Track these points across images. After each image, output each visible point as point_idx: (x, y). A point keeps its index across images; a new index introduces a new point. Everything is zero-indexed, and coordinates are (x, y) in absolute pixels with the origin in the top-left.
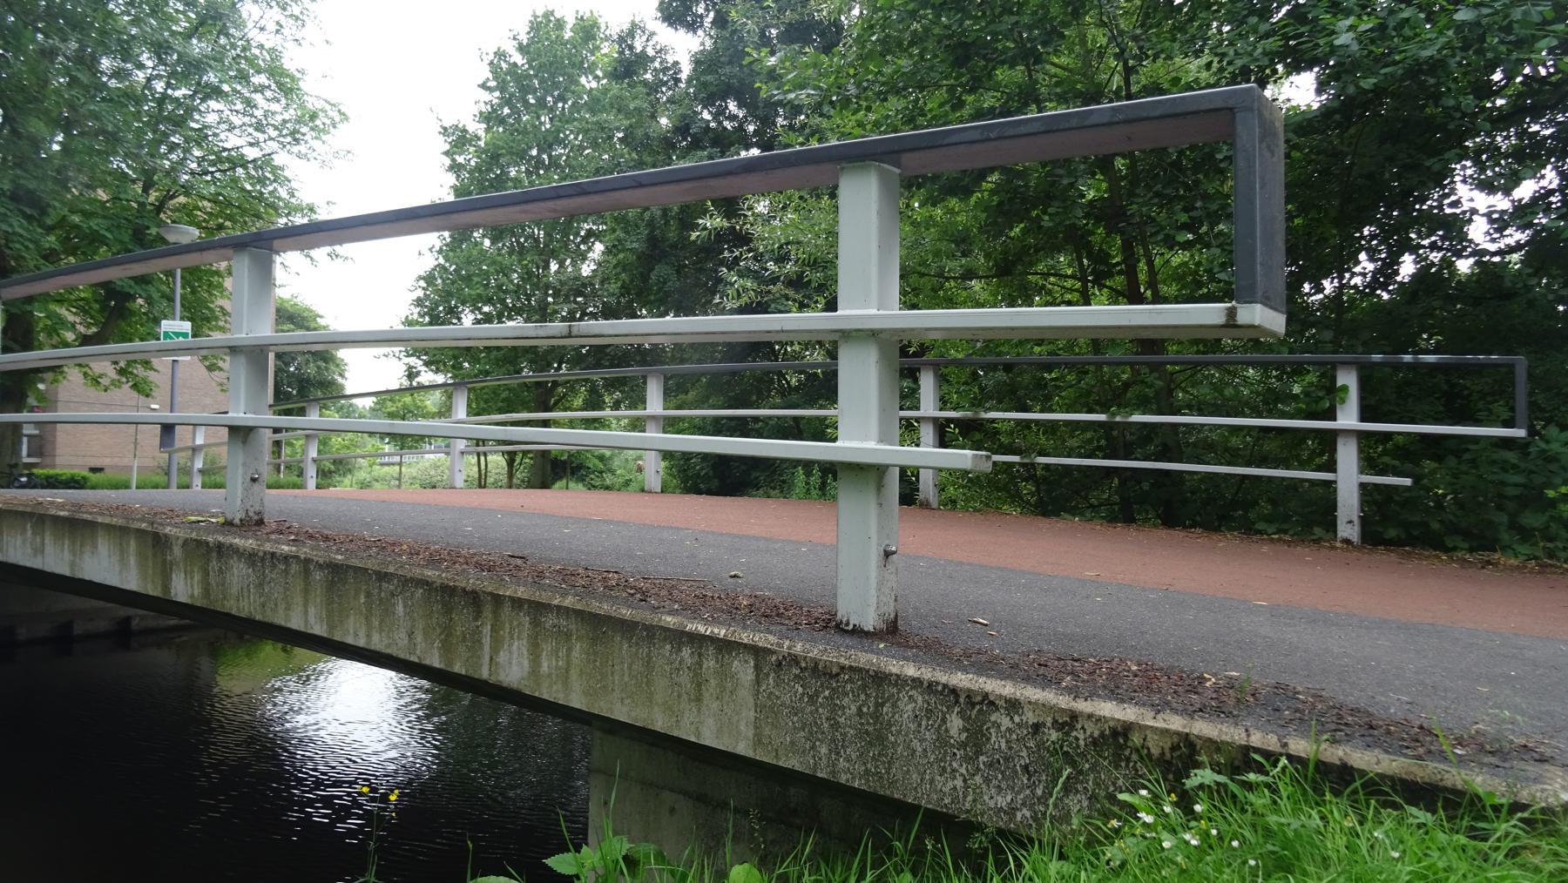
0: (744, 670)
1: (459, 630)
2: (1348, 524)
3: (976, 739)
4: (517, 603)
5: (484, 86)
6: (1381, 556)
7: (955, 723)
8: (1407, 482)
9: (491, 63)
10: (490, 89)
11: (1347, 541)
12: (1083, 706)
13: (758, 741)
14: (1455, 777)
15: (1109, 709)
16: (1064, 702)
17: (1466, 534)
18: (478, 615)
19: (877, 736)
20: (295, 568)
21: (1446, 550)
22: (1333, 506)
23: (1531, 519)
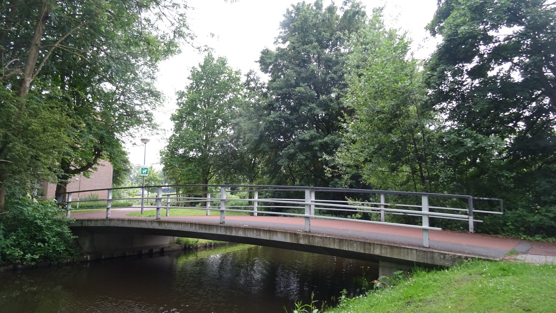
0: (415, 252)
1: (367, 248)
2: (471, 229)
3: (444, 258)
4: (378, 244)
5: (189, 78)
6: (478, 235)
7: (442, 256)
8: (482, 221)
9: (191, 71)
10: (190, 79)
11: (471, 232)
12: (456, 254)
13: (417, 259)
14: (490, 259)
15: (459, 254)
16: (454, 254)
17: (493, 231)
18: (371, 245)
19: (432, 258)
20: (331, 239)
21: (489, 234)
22: (468, 225)
23: (505, 228)
